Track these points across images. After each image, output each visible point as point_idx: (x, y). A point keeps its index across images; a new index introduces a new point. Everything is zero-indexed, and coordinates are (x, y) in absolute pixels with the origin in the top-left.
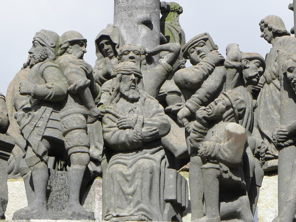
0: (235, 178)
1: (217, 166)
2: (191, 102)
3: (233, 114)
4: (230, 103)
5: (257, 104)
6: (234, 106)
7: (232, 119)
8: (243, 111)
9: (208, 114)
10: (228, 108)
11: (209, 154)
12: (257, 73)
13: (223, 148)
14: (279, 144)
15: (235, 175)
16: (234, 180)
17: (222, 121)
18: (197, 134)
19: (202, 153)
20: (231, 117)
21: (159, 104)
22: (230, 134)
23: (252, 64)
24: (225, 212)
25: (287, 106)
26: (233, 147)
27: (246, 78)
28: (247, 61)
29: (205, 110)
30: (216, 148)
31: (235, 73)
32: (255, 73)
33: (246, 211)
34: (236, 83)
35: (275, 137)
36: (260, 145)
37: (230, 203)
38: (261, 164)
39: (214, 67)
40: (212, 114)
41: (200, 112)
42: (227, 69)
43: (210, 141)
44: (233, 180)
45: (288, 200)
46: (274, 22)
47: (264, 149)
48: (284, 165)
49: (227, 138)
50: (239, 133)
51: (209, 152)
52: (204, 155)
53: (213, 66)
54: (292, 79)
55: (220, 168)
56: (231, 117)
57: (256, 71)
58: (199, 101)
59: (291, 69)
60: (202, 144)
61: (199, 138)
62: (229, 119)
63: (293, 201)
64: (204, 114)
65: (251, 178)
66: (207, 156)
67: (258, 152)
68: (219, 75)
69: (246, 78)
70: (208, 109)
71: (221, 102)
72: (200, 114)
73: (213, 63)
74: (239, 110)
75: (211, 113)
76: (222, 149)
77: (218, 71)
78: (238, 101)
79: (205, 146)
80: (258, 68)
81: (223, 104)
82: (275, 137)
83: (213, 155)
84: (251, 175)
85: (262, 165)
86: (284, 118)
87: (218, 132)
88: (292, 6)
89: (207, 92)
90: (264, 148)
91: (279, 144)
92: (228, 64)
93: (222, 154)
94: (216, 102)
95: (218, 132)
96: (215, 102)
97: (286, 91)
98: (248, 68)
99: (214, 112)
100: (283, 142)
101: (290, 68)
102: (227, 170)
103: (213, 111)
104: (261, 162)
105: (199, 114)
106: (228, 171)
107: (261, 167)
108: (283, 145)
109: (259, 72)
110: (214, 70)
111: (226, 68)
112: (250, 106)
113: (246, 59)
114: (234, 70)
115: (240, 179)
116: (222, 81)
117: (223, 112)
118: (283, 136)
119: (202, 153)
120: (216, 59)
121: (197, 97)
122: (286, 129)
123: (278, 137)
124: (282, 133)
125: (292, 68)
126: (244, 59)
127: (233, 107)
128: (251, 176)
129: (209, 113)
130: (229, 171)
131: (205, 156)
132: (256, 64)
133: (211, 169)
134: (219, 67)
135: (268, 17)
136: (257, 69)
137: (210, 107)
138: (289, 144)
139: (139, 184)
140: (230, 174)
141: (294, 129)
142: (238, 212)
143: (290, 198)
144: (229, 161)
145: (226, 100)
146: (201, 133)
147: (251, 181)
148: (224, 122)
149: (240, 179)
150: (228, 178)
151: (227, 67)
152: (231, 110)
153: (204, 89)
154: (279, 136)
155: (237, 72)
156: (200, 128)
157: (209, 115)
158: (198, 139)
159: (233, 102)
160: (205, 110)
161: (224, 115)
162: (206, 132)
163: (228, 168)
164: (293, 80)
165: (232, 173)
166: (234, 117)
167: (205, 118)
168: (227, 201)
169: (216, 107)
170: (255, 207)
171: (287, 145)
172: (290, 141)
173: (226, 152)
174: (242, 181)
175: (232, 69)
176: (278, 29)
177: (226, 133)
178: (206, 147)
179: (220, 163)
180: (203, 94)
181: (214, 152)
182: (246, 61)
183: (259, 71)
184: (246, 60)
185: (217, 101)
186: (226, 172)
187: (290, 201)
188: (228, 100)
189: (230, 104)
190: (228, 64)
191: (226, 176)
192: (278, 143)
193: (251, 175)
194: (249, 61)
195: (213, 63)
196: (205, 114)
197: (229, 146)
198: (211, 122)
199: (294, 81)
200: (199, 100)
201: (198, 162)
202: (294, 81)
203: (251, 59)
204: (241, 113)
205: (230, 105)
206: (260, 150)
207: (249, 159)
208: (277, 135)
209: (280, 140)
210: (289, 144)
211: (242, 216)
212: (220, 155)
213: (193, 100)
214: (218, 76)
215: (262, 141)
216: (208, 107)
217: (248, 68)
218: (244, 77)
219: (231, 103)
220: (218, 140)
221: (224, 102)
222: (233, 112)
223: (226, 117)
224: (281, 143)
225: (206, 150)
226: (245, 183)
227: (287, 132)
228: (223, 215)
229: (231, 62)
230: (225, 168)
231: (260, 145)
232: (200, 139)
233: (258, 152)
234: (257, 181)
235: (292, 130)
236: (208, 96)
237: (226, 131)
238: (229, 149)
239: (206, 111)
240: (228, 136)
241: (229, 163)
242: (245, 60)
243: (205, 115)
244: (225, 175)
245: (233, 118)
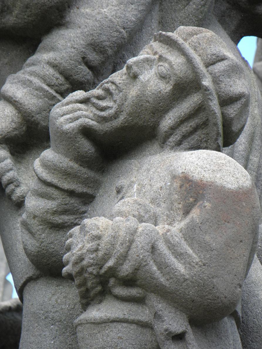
1: (143, 314)
2: (26, 83)
9: (99, 116)
11: (110, 263)
18: (54, 199)
19: (81, 259)
20: (195, 130)
22: (191, 191)
29: (85, 101)
30: (137, 239)
40: (116, 116)
41: (66, 108)
43: (111, 217)
49: (180, 206)
50: (229, 186)
51: (109, 258)
52: (90, 269)
56: (195, 130)
58: (57, 79)
60: (82, 229)
61: (62, 217)
62: (185, 137)
64: (86, 117)
66: (103, 271)
70: (99, 98)
72: (68, 116)
75: (112, 111)
76: (162, 247)
78: (219, 67)
79: (95, 233)
81: (161, 76)
83: (126, 269)
87: (143, 186)
89: (91, 44)
93: (163, 266)
94: (135, 69)
95: (143, 186)
96: (129, 68)
99: (127, 109)
103: (121, 106)
105: (62, 119)
119: (85, 263)
121: (50, 63)
129: (103, 114)
131: (95, 272)
133: (119, 326)
137: (107, 90)
139: (4, 135)
144: (192, 292)
146: (71, 193)
152: (194, 99)
153: (79, 31)
156: (66, 174)
157: (104, 120)
158: (59, 219)
160: (85, 101)
161: (167, 121)
162: (90, 191)
167: (86, 132)
169: (133, 92)
173: (180, 256)
177: (176, 185)
178: (98, 238)
180: (73, 50)
181: (129, 258)
185: (137, 63)
196: (86, 116)
197: (189, 234)
198: (112, 148)
200: (58, 75)
201: (57, 311)
205: (192, 82)
212: (155, 268)
213: (32, 74)
216: (97, 91)
220: (142, 214)
221: (164, 68)
223: (173, 129)
225: (97, 250)
232: (66, 218)
236: (94, 57)
237: (174, 177)
238: (191, 245)
239: (94, 105)
243: (87, 120)
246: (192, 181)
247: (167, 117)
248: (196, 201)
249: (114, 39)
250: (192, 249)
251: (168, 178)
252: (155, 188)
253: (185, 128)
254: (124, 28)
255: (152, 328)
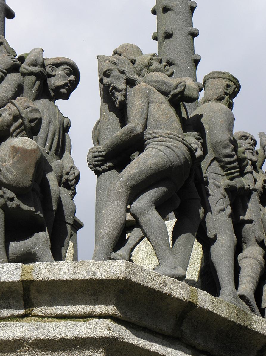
0: (24, 207)
3: (23, 126)
4: (18, 112)
5: (69, 123)
6: (22, 115)
7: (22, 133)
8: (36, 122)
10: (16, 118)
12: (67, 82)
13: (6, 168)
14: (95, 169)
15: (25, 204)
16: (24, 210)
17: (10, 137)
21: (117, 252)
22: (15, 150)
23: (60, 72)
24: (16, 254)
25: (106, 122)
26: (19, 166)
27: (52, 89)
28: (53, 68)
31: (33, 81)
32: (64, 82)
33: (43, 251)
34: (36, 94)
35: (91, 161)
36: (68, 170)
37: (22, 242)
38: (71, 195)
39: (5, 74)
42: (24, 77)
44: (23, 210)
45: (102, 235)
46: (128, 51)
47: (73, 175)
48: (102, 195)
49: (12, 156)
50: (28, 148)
53: (3, 73)
54: (110, 85)
55: (4, 194)
57: (65, 80)
59: (107, 72)
63: (108, 236)
65: (54, 211)
67: (67, 180)
68: (12, 84)
69: (52, 89)
71: (7, 113)
73: (3, 69)
74: (31, 121)
77: (11, 78)
80: (67, 76)
82: (91, 161)
84: (55, 207)
85: (73, 196)
86: (103, 137)
88: (157, 35)
90: (74, 173)
91: (95, 169)
92: (24, 70)
97: (106, 103)
98: (54, 75)
100: (99, 166)
101: (106, 71)
102: (12, 197)
104: (71, 192)
106: (13, 198)
107: (71, 199)
108: (100, 169)
109: (70, 81)
110: (6, 78)
111: (22, 75)
112: (57, 124)
113: (52, 65)
114: (33, 78)
115: (32, 209)
116: (16, 91)
117: (9, 125)
118: (98, 158)
120: (7, 64)
122: (102, 148)
123: (93, 160)
124: (97, 154)
125: (109, 71)
126: (49, 65)
127: (21, 117)
128: (54, 209)
130: (16, 198)
132: (64, 71)
134: (12, 74)
135: (122, 46)
136: (66, 77)
138: (107, 168)
140: (17, 201)
141: (111, 147)
142: (34, 253)
143: (103, 232)
144: (14, 184)
145: (12, 108)
147: (54, 215)
148: (12, 138)
149: (32, 209)
150: (15, 207)
151: (24, 75)
152: (20, 121)
154: (94, 158)
155: (37, 80)
159: (21, 110)
161: (12, 129)
163: (14, 194)
164: (111, 87)
165: (21, 201)
166: (25, 131)
168: (18, 240)
170: (64, 251)
171: (105, 169)
172: (109, 164)
173: (10, 172)
174: (36, 211)
175: (30, 77)
176: (133, 58)
179: (3, 188)
182: (51, 68)
183: (68, 79)
184: (51, 66)
186: (12, 200)
187: (103, 237)
188: (15, 108)
189: (18, 113)
190: (24, 70)
191: (12, 205)
192: (94, 168)
193: (55, 207)
194: (55, 67)
195: (3, 69)
197: (13, 165)
199: (112, 88)
202: (112, 88)
203: (58, 65)
204: (33, 125)
205: (19, 115)
206: (68, 176)
207: (51, 187)
208: (92, 157)
209: (96, 163)
210: (107, 168)
211: (38, 257)
214: (10, 85)
215: (71, 166)
217: (54, 75)
218: (49, 87)
219: (20, 113)
222: (23, 124)
223: (14, 131)
224: (98, 168)
226: (42, 215)
227: (103, 152)
228: (13, 258)
229: (28, 68)
230: (10, 194)
231: (68, 170)
233: (66, 179)
234: (66, 217)
235: (110, 149)
238: (13, 169)
240: (13, 153)
241: (15, 187)
242: (49, 66)
244: (10, 204)
245: (24, 132)
246: (15, 148)
247: (12, 127)
248: (16, 154)
249: (4, 103)
250: (14, 170)
251: (9, 147)
252: (6, 151)
253: (18, 131)
254: (7, 100)
255: (3, 197)
